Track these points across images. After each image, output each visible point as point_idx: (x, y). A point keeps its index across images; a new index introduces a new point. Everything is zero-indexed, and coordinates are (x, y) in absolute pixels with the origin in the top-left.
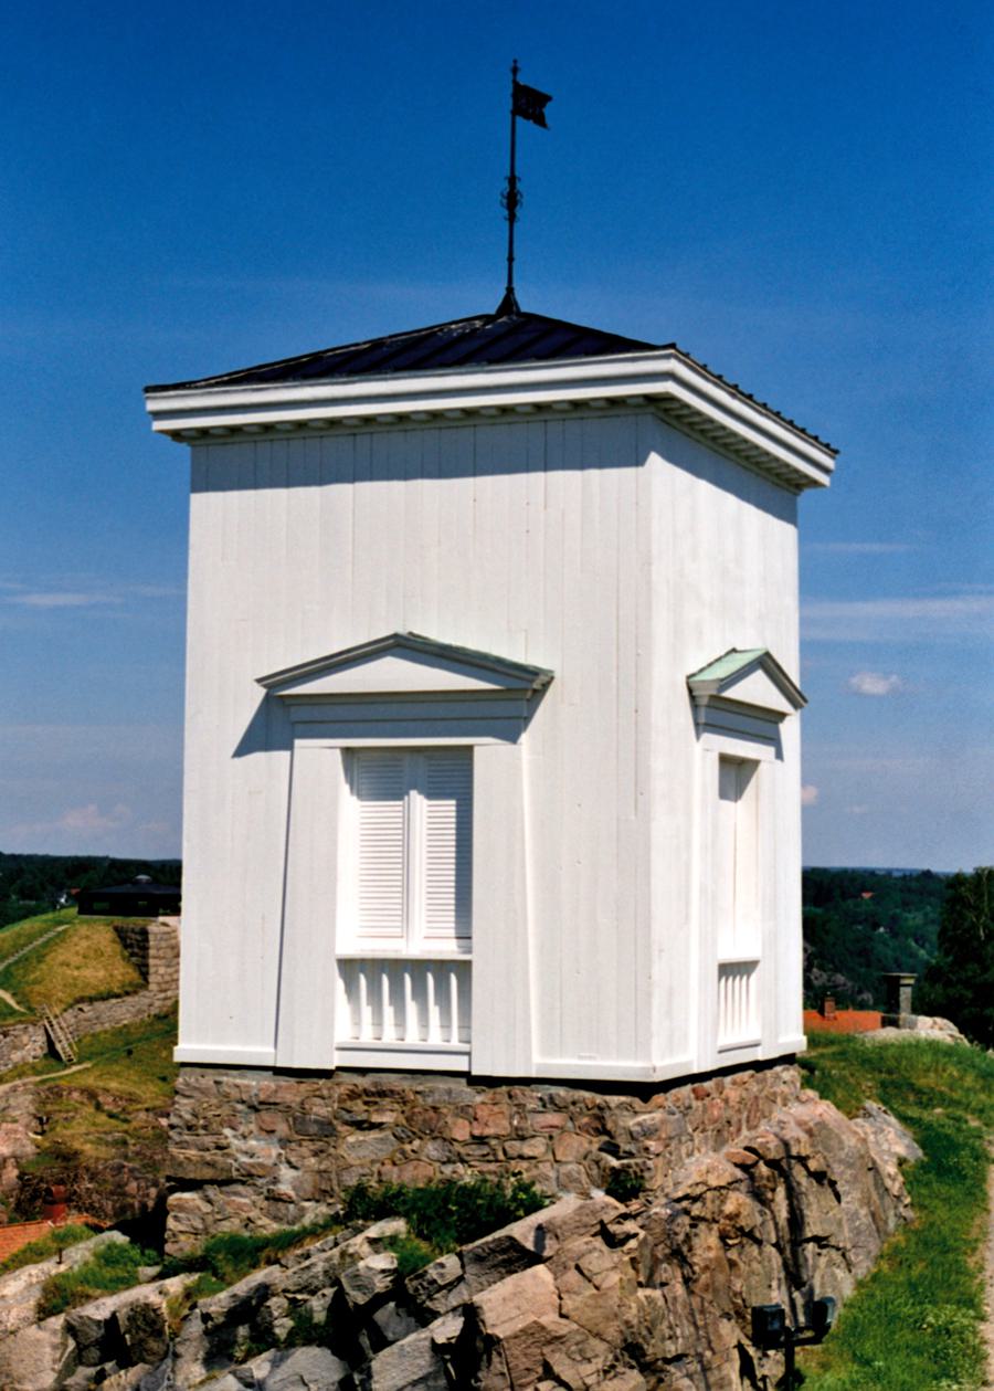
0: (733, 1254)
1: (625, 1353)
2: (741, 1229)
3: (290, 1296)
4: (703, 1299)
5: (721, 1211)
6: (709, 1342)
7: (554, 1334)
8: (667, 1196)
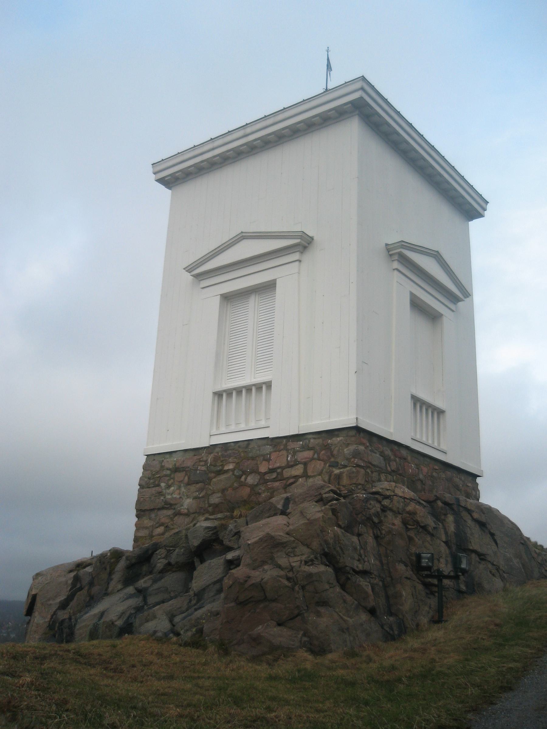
2: (417, 522)
5: (404, 510)
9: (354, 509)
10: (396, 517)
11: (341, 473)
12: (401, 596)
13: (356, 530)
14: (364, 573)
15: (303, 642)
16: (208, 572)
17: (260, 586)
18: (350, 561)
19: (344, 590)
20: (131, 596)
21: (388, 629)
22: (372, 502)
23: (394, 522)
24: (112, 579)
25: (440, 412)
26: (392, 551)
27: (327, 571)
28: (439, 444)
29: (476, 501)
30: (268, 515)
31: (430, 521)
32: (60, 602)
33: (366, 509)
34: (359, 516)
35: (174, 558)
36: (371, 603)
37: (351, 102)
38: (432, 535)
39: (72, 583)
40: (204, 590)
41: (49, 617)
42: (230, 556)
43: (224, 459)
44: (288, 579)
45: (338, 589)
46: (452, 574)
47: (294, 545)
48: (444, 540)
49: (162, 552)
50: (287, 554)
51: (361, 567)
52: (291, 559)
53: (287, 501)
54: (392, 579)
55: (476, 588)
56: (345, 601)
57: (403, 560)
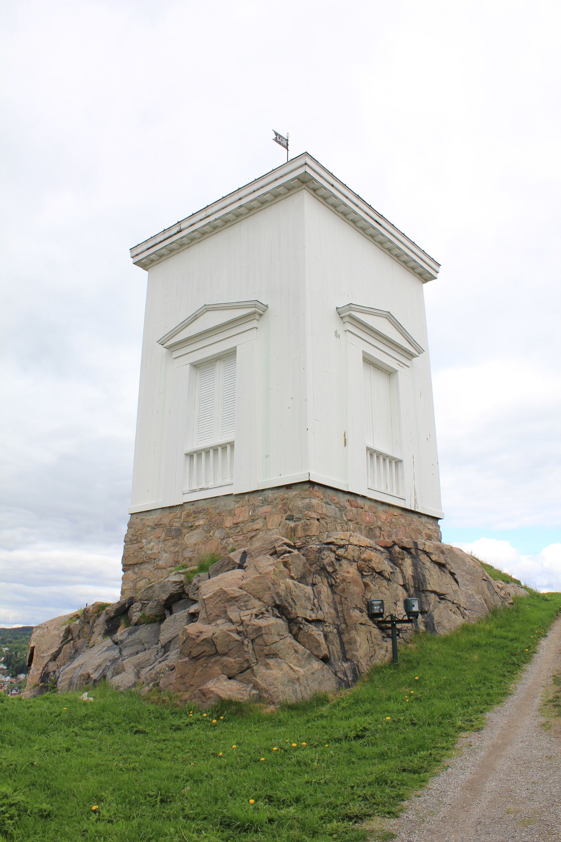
0: (367, 580)
1: (274, 609)
2: (373, 569)
3: (143, 602)
4: (341, 597)
5: (360, 557)
6: (345, 620)
7: (231, 595)
8: (320, 541)
9: (307, 560)
10: (351, 565)
11: (296, 526)
12: (355, 642)
13: (310, 580)
14: (318, 622)
15: (251, 695)
16: (175, 624)
17: (210, 642)
18: (302, 611)
19: (297, 640)
20: (109, 648)
21: (342, 676)
22: (325, 553)
23: (349, 571)
24: (93, 633)
25: (398, 462)
26: (346, 598)
27: (277, 623)
28: (398, 493)
29: (438, 543)
30: (227, 569)
31: (386, 567)
32: (52, 654)
33: (320, 560)
34: (314, 566)
35: (148, 611)
36: (324, 651)
37: (297, 178)
38: (389, 580)
39: (63, 636)
40: (170, 642)
41: (41, 669)
42: (193, 609)
43: (195, 515)
44: (239, 633)
45: (290, 640)
46: (406, 618)
47: (246, 599)
48: (402, 584)
49: (136, 606)
50: (239, 608)
51: (314, 616)
52: (242, 613)
53: (245, 554)
54: (347, 626)
55: (436, 627)
56: (296, 652)
57: (359, 606)
